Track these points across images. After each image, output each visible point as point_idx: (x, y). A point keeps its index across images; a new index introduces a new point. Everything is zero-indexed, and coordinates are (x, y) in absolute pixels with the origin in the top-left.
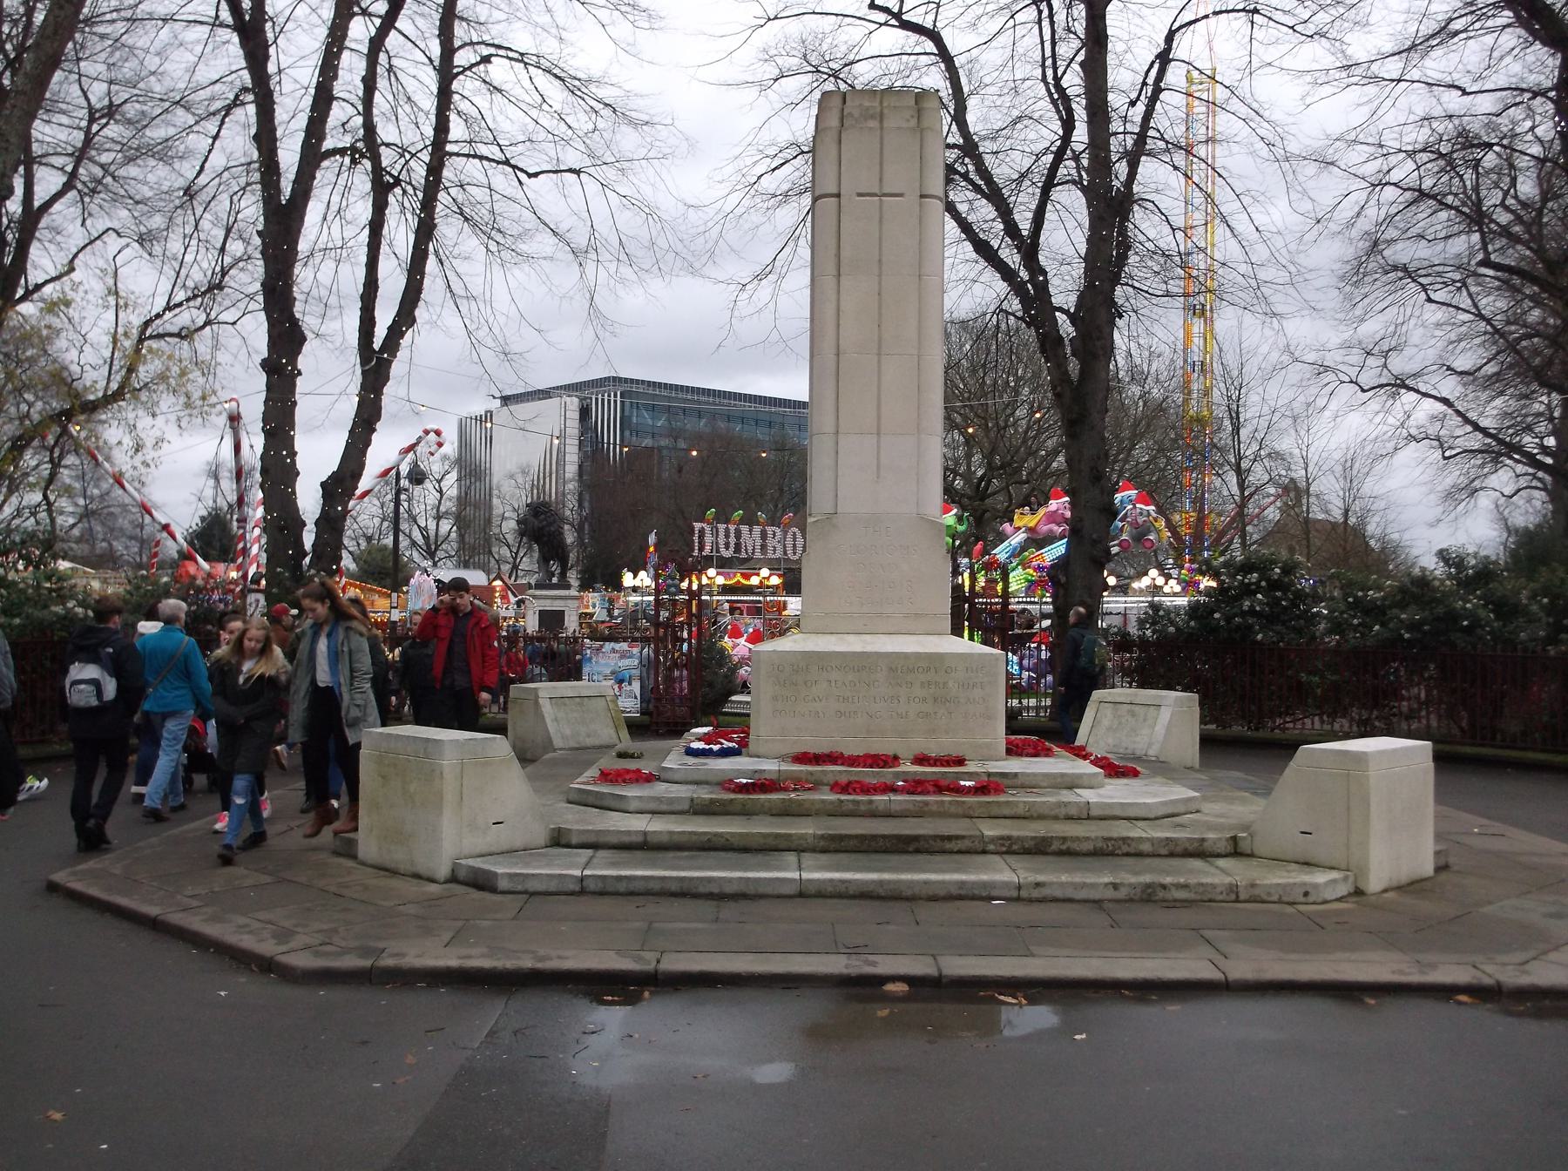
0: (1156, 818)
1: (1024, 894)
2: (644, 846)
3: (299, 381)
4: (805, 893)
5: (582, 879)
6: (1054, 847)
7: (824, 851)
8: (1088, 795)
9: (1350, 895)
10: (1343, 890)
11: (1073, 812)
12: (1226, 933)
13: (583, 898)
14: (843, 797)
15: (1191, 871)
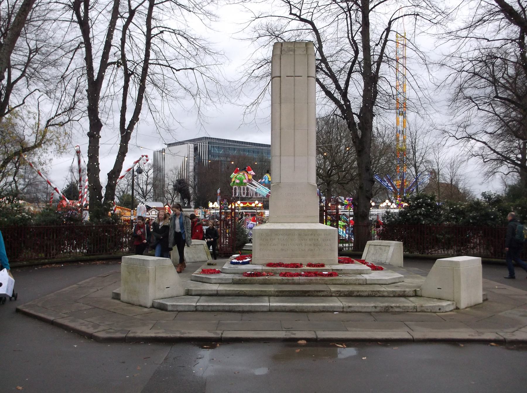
0: (389, 284)
1: (345, 310)
2: (217, 295)
3: (100, 139)
4: (271, 310)
5: (196, 306)
6: (355, 294)
7: (277, 296)
8: (366, 276)
9: (454, 309)
10: (452, 308)
11: (361, 282)
12: (413, 323)
13: (196, 313)
14: (284, 278)
15: (401, 302)
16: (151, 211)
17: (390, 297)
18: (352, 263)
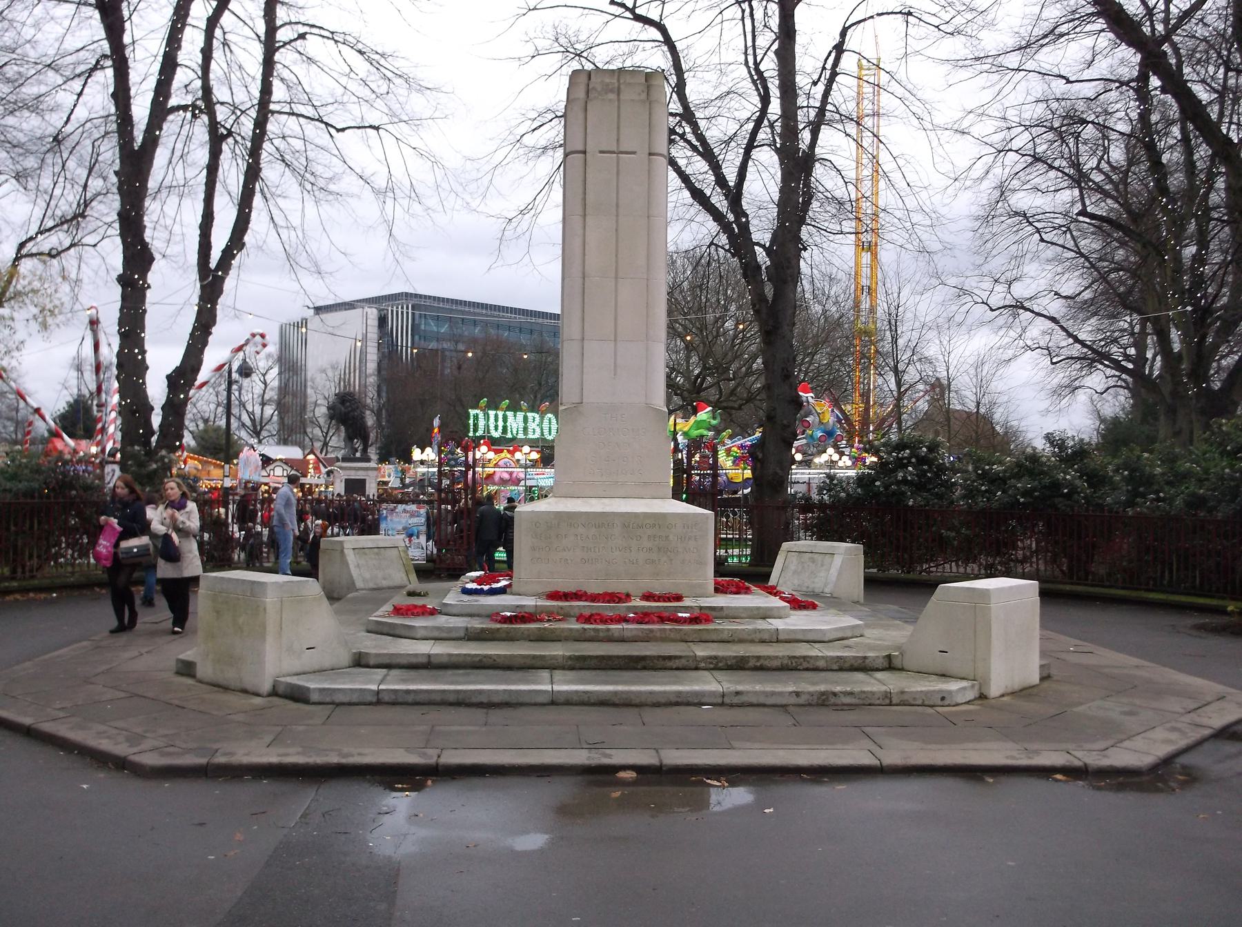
1: (727, 700)
2: (428, 665)
3: (149, 293)
4: (555, 701)
5: (378, 692)
7: (572, 668)
9: (975, 699)
10: (971, 695)
11: (766, 637)
13: (379, 708)
16: (271, 467)
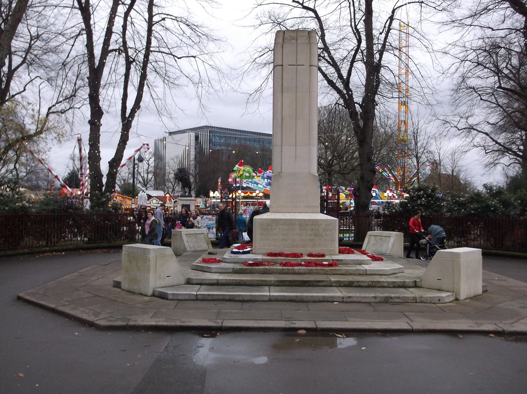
1: (345, 300)
3: (101, 127)
4: (271, 300)
5: (197, 295)
7: (278, 286)
9: (454, 300)
10: (452, 299)
11: (361, 273)
13: (197, 302)
14: (284, 268)
15: (401, 293)
16: (152, 199)
17: (390, 287)
18: (352, 254)
